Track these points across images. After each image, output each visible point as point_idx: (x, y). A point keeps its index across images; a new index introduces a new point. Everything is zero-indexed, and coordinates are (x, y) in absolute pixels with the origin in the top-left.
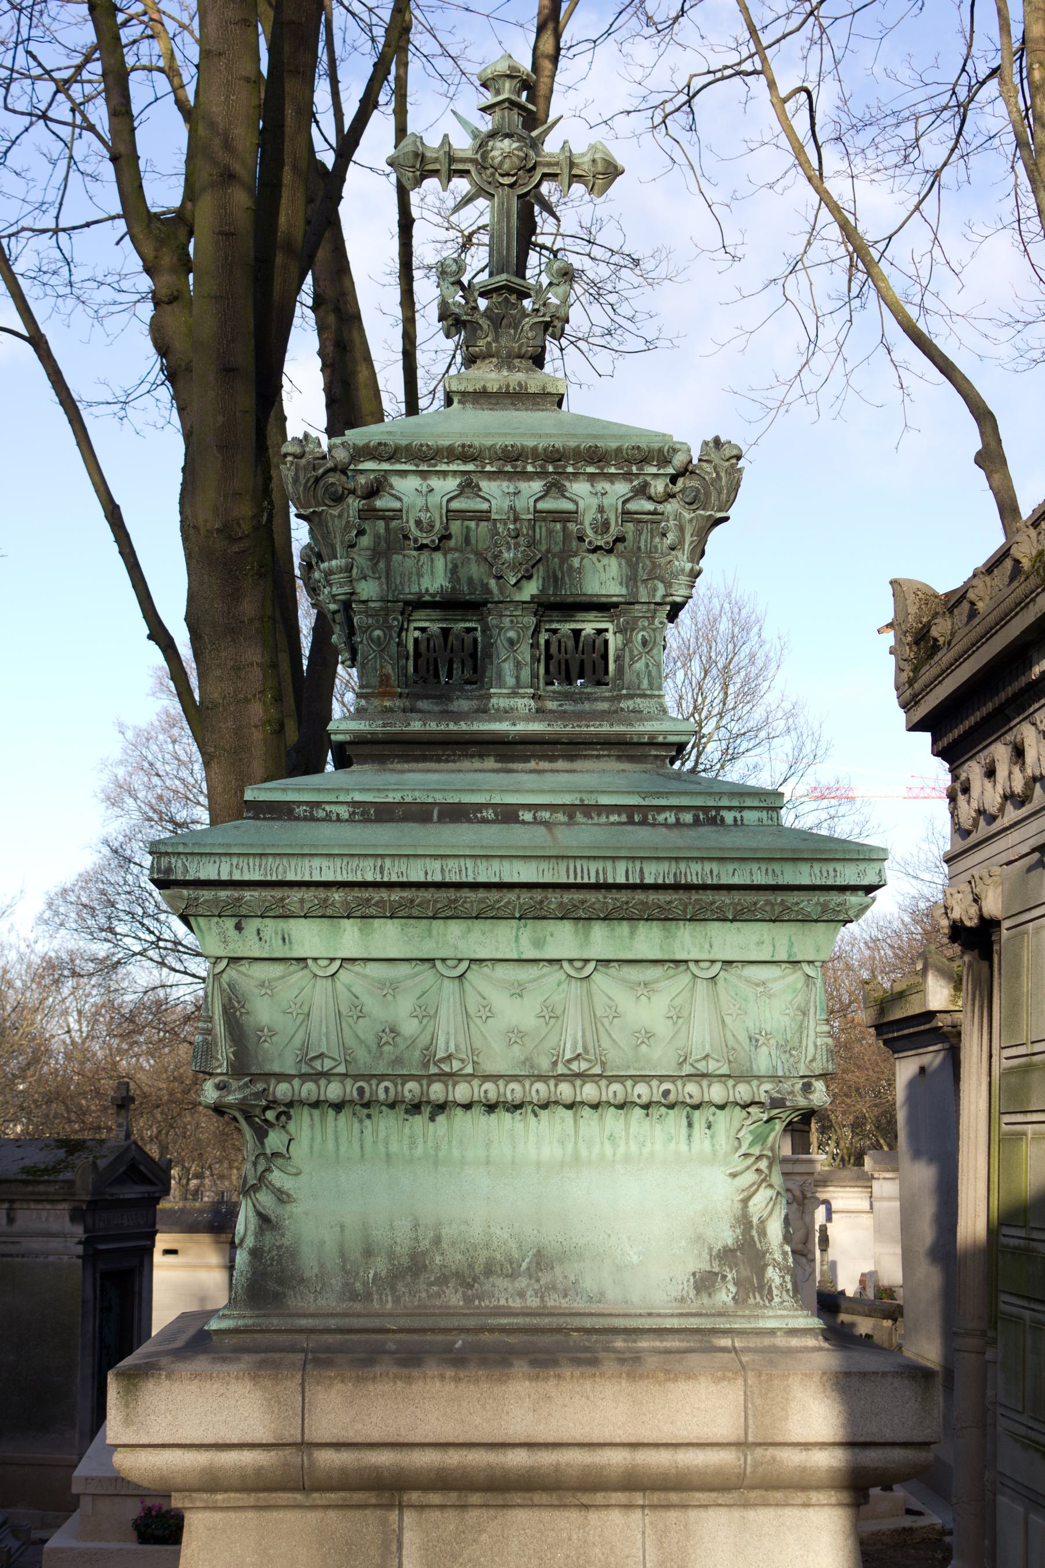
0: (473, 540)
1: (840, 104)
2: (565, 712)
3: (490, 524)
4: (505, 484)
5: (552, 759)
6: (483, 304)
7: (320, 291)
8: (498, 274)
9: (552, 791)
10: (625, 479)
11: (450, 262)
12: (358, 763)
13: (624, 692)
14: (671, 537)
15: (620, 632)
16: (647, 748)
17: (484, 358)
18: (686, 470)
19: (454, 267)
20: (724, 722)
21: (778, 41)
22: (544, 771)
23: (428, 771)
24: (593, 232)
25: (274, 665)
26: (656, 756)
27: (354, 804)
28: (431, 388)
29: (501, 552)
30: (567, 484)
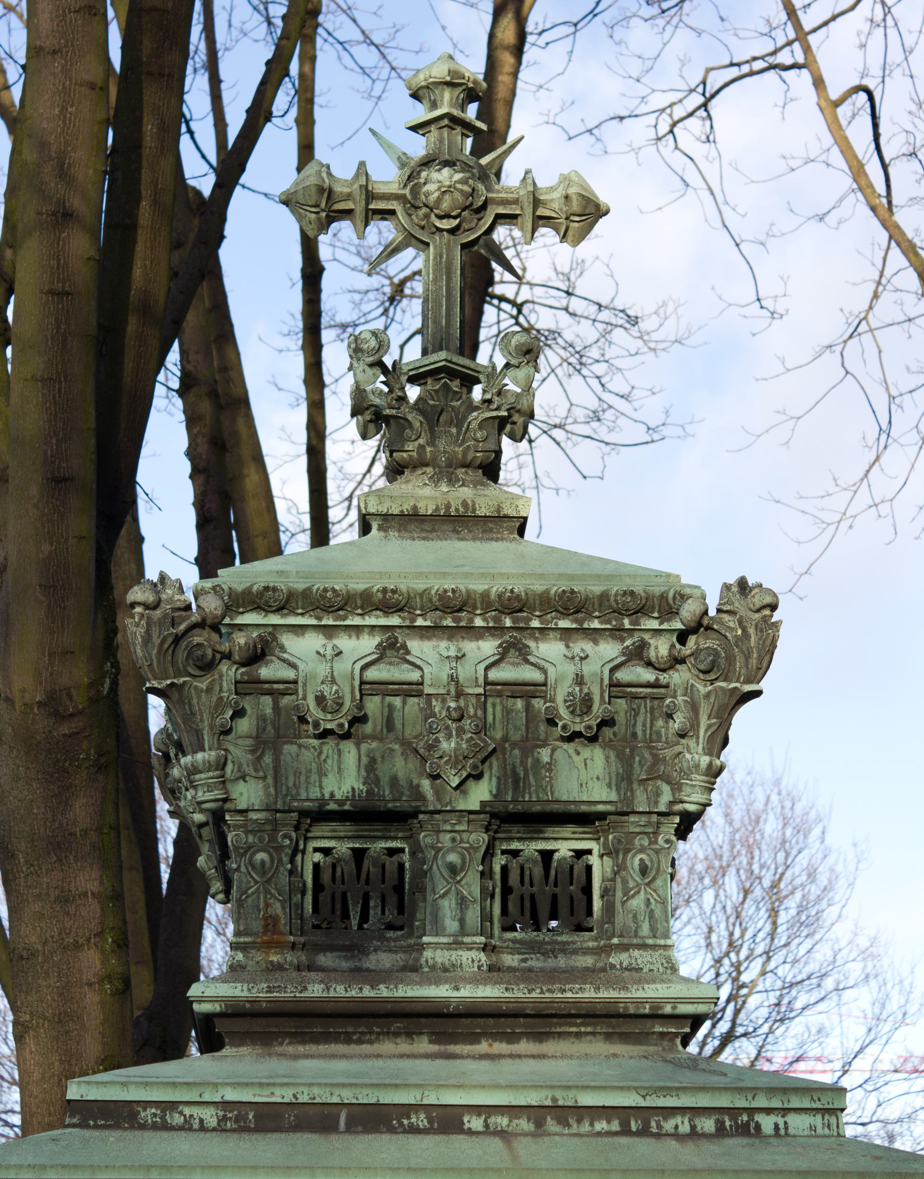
0: (398, 724)
1: (914, 108)
2: (530, 970)
3: (422, 701)
4: (444, 644)
5: (512, 1038)
6: (413, 393)
7: (189, 367)
8: (434, 351)
9: (511, 1087)
10: (614, 638)
11: (367, 336)
12: (232, 1045)
13: (615, 941)
14: (679, 720)
15: (609, 854)
16: (649, 1022)
17: (415, 467)
18: (700, 624)
19: (373, 343)
20: (772, 965)
21: (826, 24)
22: (500, 1056)
23: (333, 1056)
24: (572, 278)
25: (117, 896)
26: (662, 1034)
27: (225, 1105)
28: (347, 494)
29: (437, 740)
30: (532, 644)
